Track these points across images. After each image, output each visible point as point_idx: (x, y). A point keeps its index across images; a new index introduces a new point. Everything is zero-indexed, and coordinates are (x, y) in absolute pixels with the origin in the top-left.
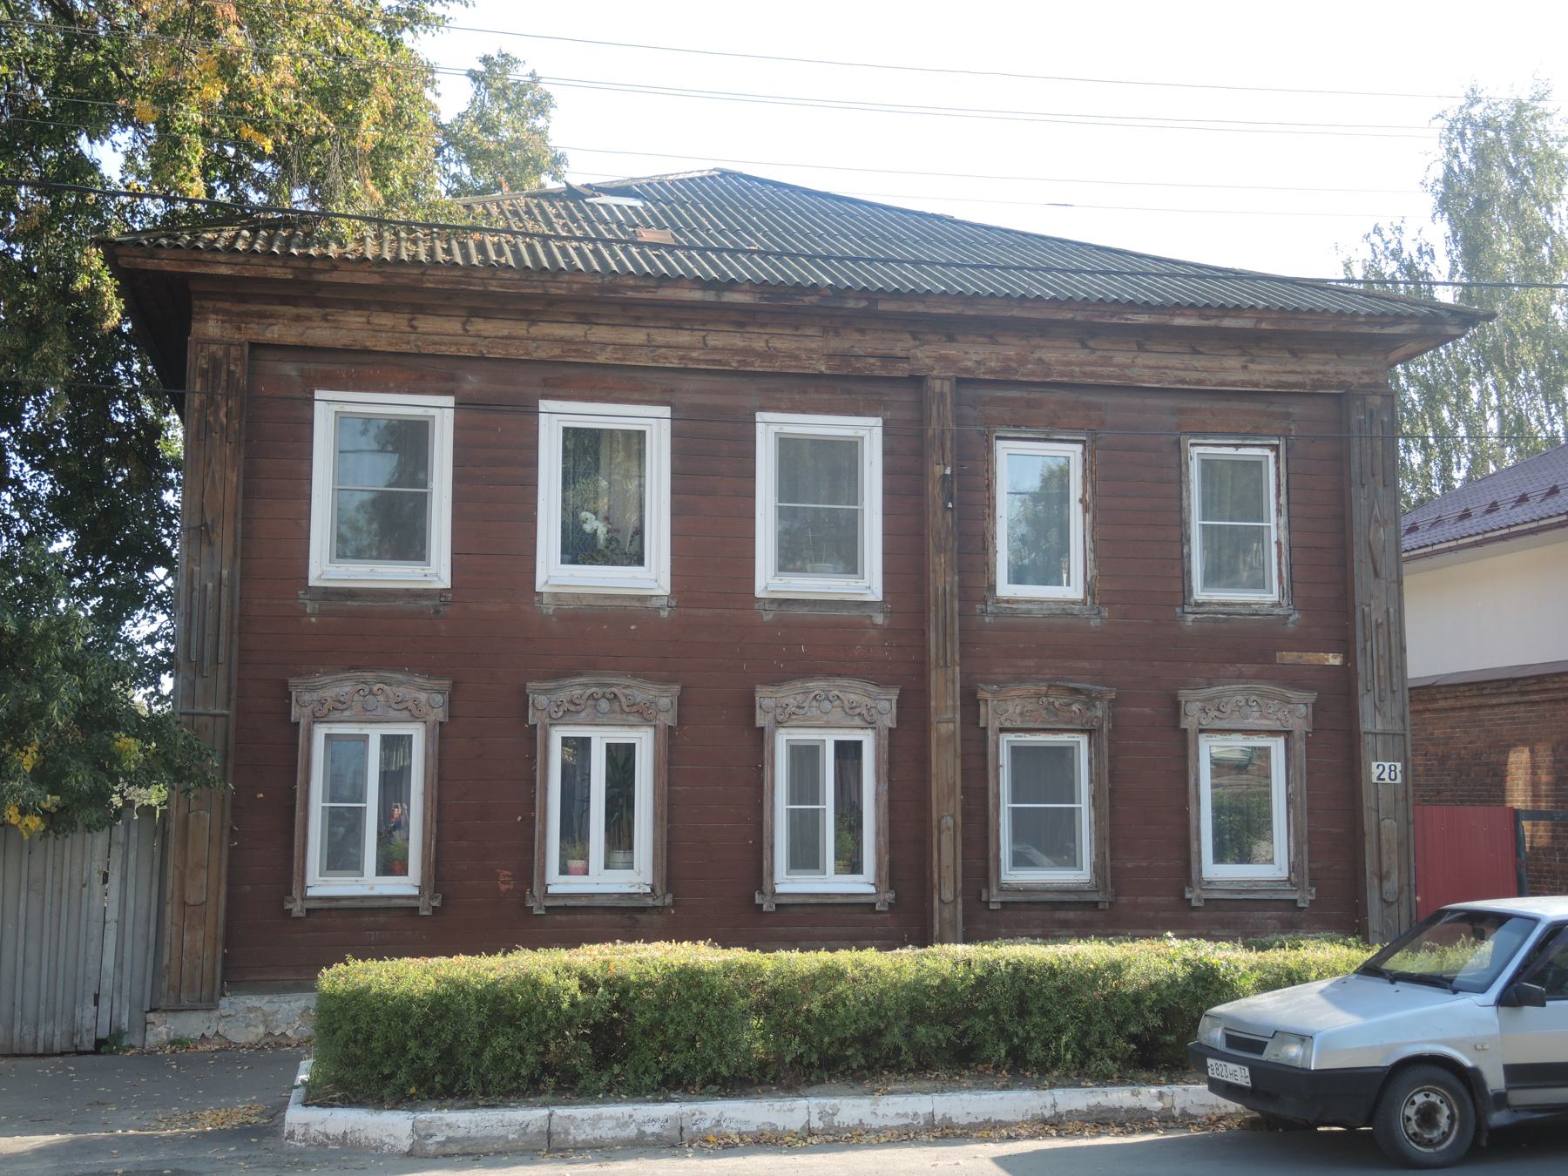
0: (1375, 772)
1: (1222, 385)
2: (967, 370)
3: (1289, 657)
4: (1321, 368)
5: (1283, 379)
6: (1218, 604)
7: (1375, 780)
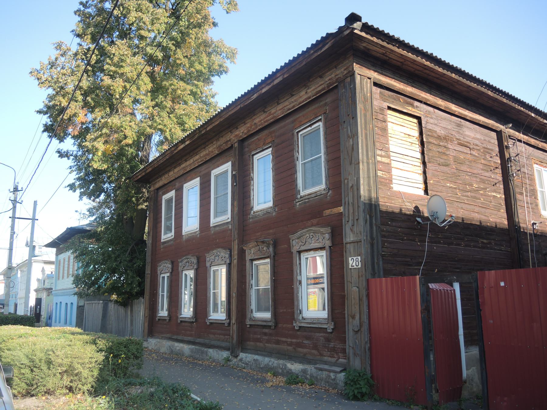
0: (351, 262)
1: (300, 104)
2: (241, 137)
3: (327, 212)
4: (330, 77)
5: (318, 90)
6: (308, 195)
7: (350, 267)
